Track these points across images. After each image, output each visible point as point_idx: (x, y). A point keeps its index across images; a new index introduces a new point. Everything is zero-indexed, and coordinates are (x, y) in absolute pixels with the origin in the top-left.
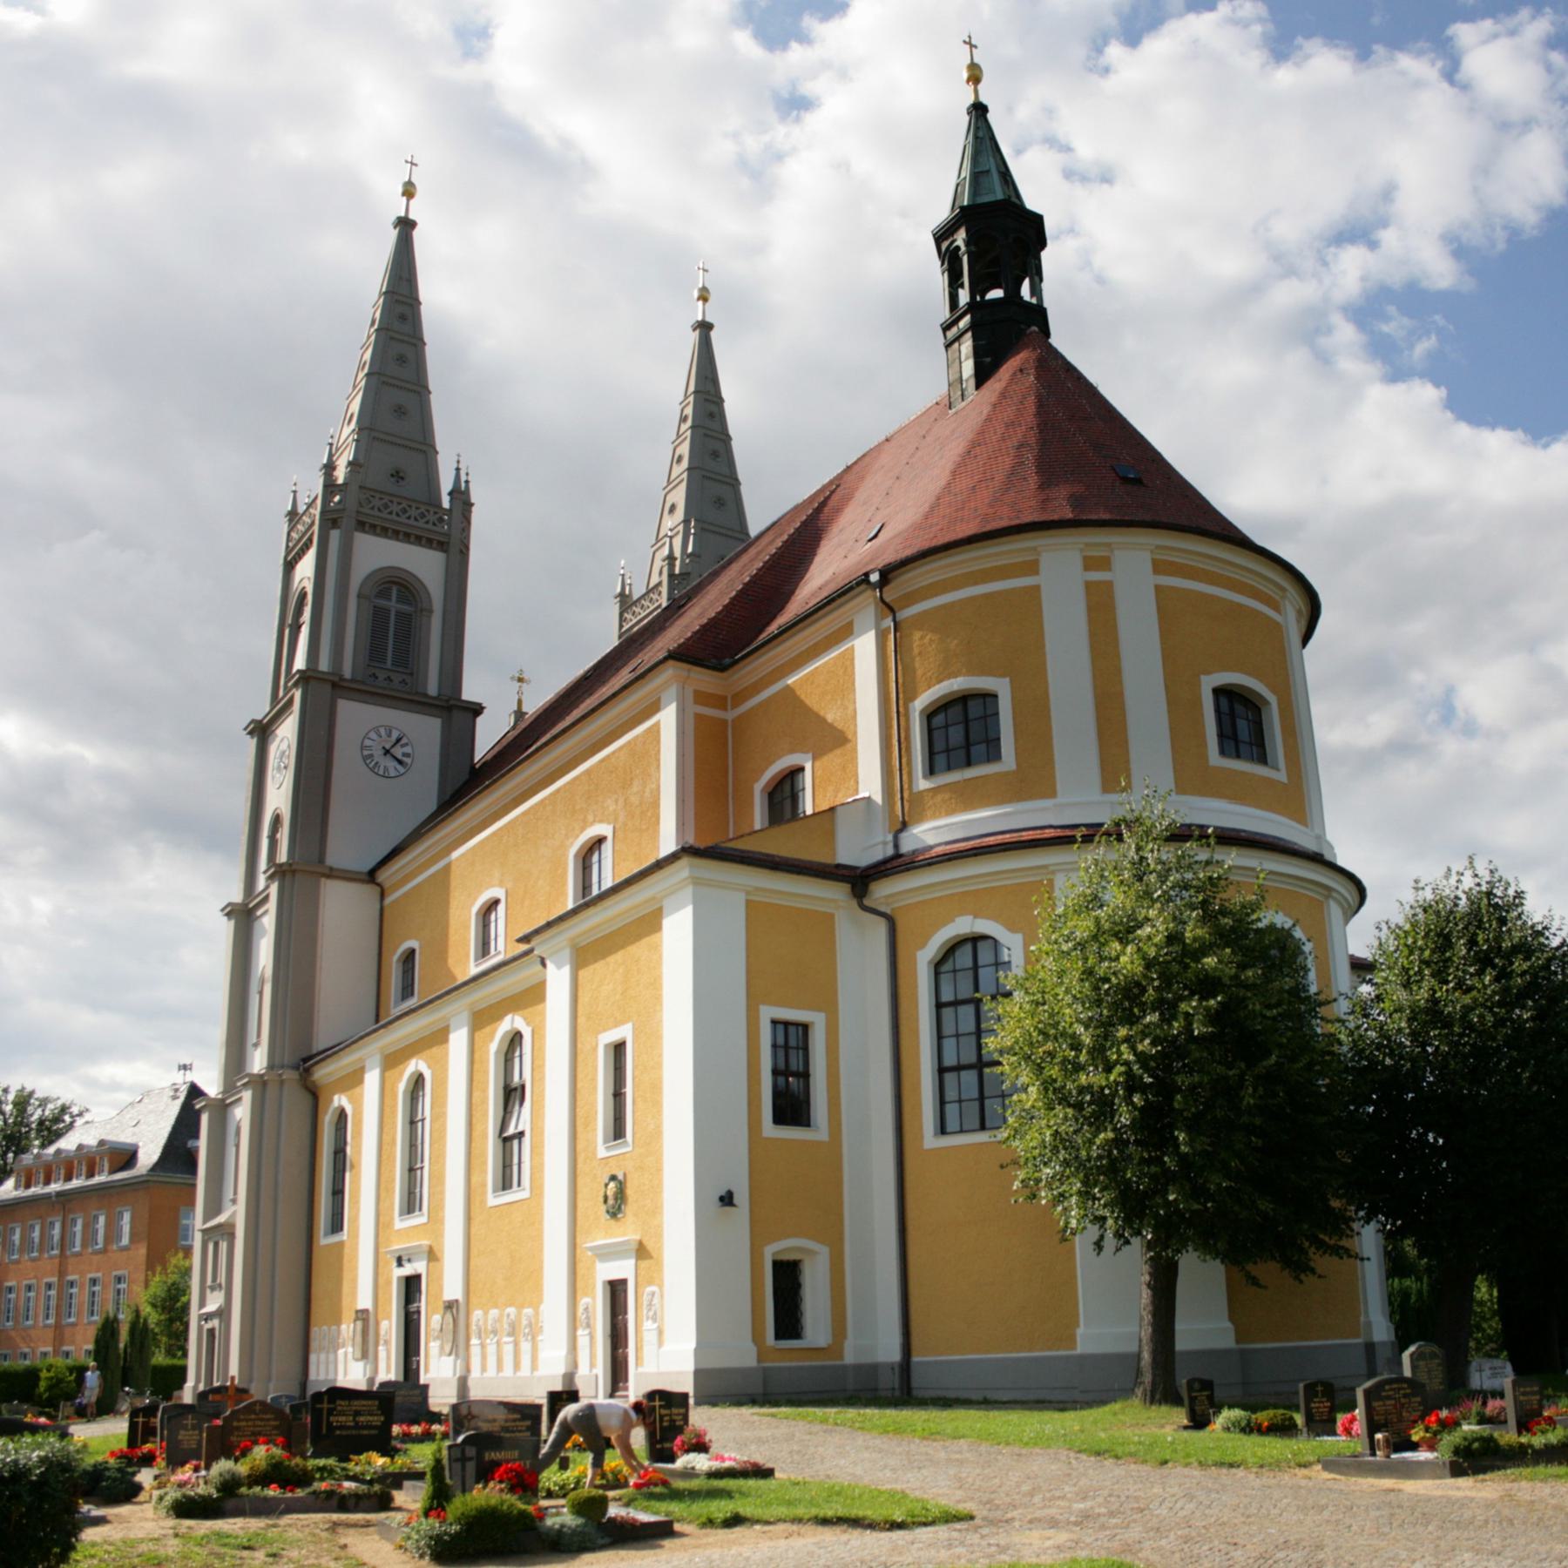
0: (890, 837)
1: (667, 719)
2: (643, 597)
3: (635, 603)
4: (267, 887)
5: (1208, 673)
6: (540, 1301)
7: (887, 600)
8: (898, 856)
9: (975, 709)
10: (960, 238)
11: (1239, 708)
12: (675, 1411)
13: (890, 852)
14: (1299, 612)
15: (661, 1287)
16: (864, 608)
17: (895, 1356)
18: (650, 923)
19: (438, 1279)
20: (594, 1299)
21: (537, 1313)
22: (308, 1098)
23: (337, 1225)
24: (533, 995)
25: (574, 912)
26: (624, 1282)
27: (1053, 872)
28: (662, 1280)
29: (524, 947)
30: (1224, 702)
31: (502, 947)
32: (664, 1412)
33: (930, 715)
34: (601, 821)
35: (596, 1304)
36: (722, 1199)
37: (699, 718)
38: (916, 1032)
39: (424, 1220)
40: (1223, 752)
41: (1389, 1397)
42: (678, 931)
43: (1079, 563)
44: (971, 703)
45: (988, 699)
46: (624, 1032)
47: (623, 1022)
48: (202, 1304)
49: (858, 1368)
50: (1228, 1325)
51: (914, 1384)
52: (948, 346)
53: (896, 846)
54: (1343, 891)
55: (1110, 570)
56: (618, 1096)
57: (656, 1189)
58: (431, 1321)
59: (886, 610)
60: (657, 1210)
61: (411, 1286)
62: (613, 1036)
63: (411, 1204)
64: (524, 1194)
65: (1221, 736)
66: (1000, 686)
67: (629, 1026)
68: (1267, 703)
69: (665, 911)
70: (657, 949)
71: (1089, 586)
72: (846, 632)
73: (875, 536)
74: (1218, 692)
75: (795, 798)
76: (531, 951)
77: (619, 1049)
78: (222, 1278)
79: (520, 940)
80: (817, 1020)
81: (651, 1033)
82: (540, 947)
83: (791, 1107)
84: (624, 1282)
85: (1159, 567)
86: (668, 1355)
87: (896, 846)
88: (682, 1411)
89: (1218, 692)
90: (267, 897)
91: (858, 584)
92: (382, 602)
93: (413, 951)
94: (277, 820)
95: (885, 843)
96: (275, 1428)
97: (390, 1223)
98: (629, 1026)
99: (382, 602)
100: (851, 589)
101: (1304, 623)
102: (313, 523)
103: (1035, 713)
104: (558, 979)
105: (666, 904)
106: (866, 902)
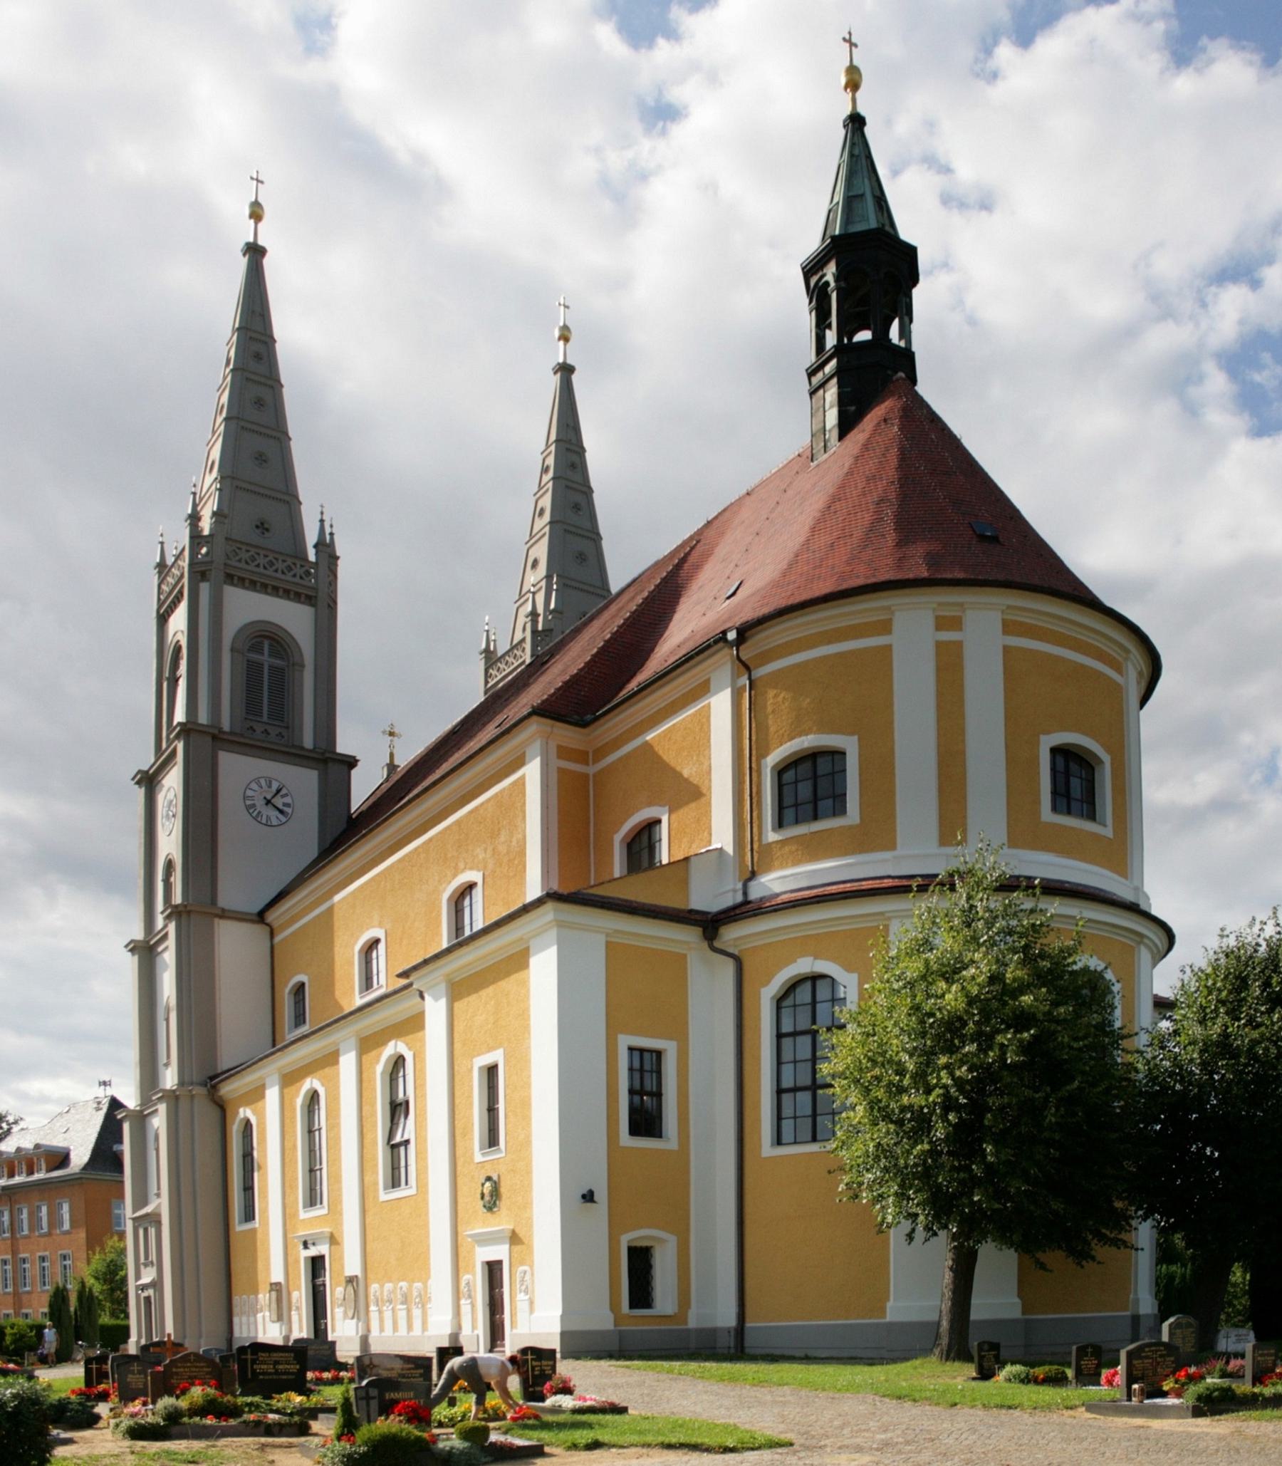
0: (740, 886)
1: (532, 772)
2: (507, 653)
3: (499, 659)
4: (165, 926)
5: (1048, 732)
6: (428, 1277)
7: (744, 658)
8: (746, 902)
9: (824, 766)
11: (1074, 767)
12: (544, 1363)
13: (739, 898)
14: (1140, 674)
15: (531, 1267)
16: (721, 666)
18: (518, 961)
20: (474, 1275)
23: (249, 1215)
24: (415, 1023)
25: (449, 951)
26: (500, 1263)
27: (889, 919)
29: (404, 982)
30: (1060, 761)
33: (781, 771)
34: (471, 869)
35: (477, 1281)
36: (584, 1196)
39: (325, 1211)
40: (1055, 809)
41: (1147, 1357)
42: (544, 968)
43: (930, 621)
44: (820, 760)
45: (836, 757)
46: (496, 1056)
48: (138, 1277)
50: (1017, 1300)
53: (745, 893)
56: (492, 1110)
57: (527, 1188)
58: (335, 1294)
59: (742, 669)
60: (527, 1205)
61: (317, 1264)
63: (313, 1199)
64: (412, 1191)
65: (1055, 793)
66: (849, 744)
68: (1101, 762)
70: (525, 984)
71: (939, 645)
72: (703, 690)
73: (734, 594)
74: (1055, 751)
75: (652, 848)
76: (410, 985)
78: (153, 1256)
79: (400, 976)
82: (419, 981)
83: (645, 1121)
84: (500, 1263)
85: (1009, 628)
86: (538, 1318)
87: (745, 893)
89: (1055, 751)
90: (166, 934)
91: (716, 642)
92: (255, 657)
93: (302, 985)
96: (207, 1373)
97: (296, 1214)
99: (255, 657)
100: (709, 647)
101: (1144, 685)
102: (182, 576)
104: (435, 1010)
105: (533, 944)
106: (717, 944)
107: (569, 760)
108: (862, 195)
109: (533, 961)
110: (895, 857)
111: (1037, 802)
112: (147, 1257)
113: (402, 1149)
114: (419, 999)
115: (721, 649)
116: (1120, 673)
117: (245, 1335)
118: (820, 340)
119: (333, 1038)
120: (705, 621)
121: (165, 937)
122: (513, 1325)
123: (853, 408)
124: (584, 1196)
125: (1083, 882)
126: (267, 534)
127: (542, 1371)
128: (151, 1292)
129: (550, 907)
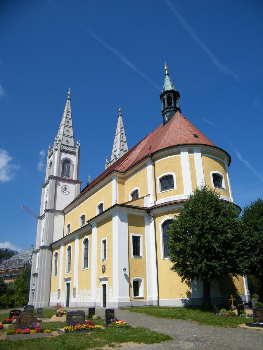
5: (212, 171)
6: (91, 288)
7: (153, 159)
10: (165, 97)
12: (112, 313)
13: (154, 205)
14: (227, 160)
17: (157, 299)
18: (110, 219)
19: (73, 284)
21: (90, 290)
22: (155, 200)
23: (56, 273)
24: (89, 233)
28: (112, 285)
31: (86, 223)
32: (109, 313)
33: (161, 180)
36: (124, 270)
37: (119, 181)
38: (159, 238)
41: (259, 310)
47: (106, 237)
48: (32, 288)
49: (149, 301)
51: (160, 304)
52: (163, 115)
53: (155, 204)
54: (236, 209)
55: (106, 285)
56: (105, 250)
57: (111, 268)
58: (71, 292)
61: (68, 285)
62: (104, 239)
67: (107, 237)
69: (113, 216)
70: (112, 223)
72: (145, 166)
76: (89, 224)
77: (104, 242)
80: (141, 236)
81: (111, 237)
83: (136, 251)
87: (155, 204)
88: (113, 313)
90: (45, 215)
93: (70, 224)
94: (46, 202)
95: (153, 203)
98: (107, 237)
101: (228, 163)
102: (49, 152)
103: (180, 179)
104: (94, 230)
105: (113, 215)
106: (150, 214)
107: (120, 179)
108: (169, 85)
109: (113, 218)
110: (184, 196)
111: (135, 233)
112: (34, 282)
113: (62, 251)
114: (91, 227)
115: (148, 158)
116: (224, 160)
117: (57, 299)
118: (164, 107)
119: (60, 243)
120: (146, 153)
121: (44, 216)
122: (108, 301)
123: (170, 117)
124: (124, 270)
125: (163, 255)
126: (68, 143)
127: (111, 315)
128: (34, 291)
129: (117, 207)
